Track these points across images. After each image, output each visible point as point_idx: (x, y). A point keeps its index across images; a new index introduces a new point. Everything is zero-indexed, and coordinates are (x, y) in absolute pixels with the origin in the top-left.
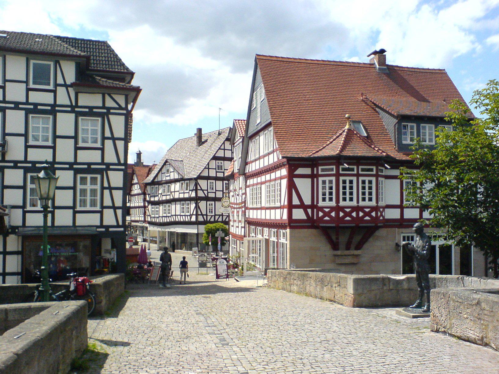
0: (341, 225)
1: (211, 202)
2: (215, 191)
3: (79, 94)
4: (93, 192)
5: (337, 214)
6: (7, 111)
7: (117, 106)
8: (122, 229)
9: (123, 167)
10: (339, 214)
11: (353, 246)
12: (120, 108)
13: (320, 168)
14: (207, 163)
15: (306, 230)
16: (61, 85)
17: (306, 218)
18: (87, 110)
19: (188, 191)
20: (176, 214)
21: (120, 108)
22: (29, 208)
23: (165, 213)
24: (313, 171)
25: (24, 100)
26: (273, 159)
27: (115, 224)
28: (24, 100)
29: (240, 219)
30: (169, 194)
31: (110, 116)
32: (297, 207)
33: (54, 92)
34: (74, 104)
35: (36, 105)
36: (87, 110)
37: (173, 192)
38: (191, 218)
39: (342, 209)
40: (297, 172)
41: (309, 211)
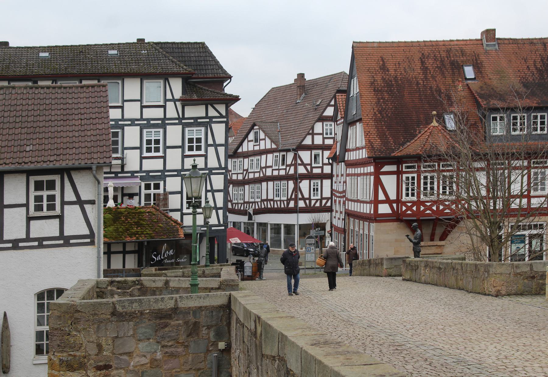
0: (421, 218)
1: (316, 181)
2: (321, 165)
3: (186, 107)
5: (418, 208)
6: (125, 127)
7: (219, 115)
8: (223, 228)
9: (224, 171)
10: (420, 208)
11: (437, 237)
12: (221, 116)
13: (404, 165)
14: (310, 127)
15: (391, 223)
16: (170, 100)
17: (391, 212)
18: (192, 121)
19: (284, 167)
20: (269, 198)
21: (221, 116)
23: (252, 198)
24: (398, 168)
25: (139, 117)
26: (363, 154)
27: (217, 223)
28: (139, 117)
29: (341, 210)
30: (259, 170)
31: (213, 125)
32: (382, 202)
33: (164, 107)
34: (181, 117)
35: (148, 120)
36: (192, 121)
37: (264, 168)
38: (288, 204)
39: (423, 203)
40: (384, 170)
41: (395, 205)
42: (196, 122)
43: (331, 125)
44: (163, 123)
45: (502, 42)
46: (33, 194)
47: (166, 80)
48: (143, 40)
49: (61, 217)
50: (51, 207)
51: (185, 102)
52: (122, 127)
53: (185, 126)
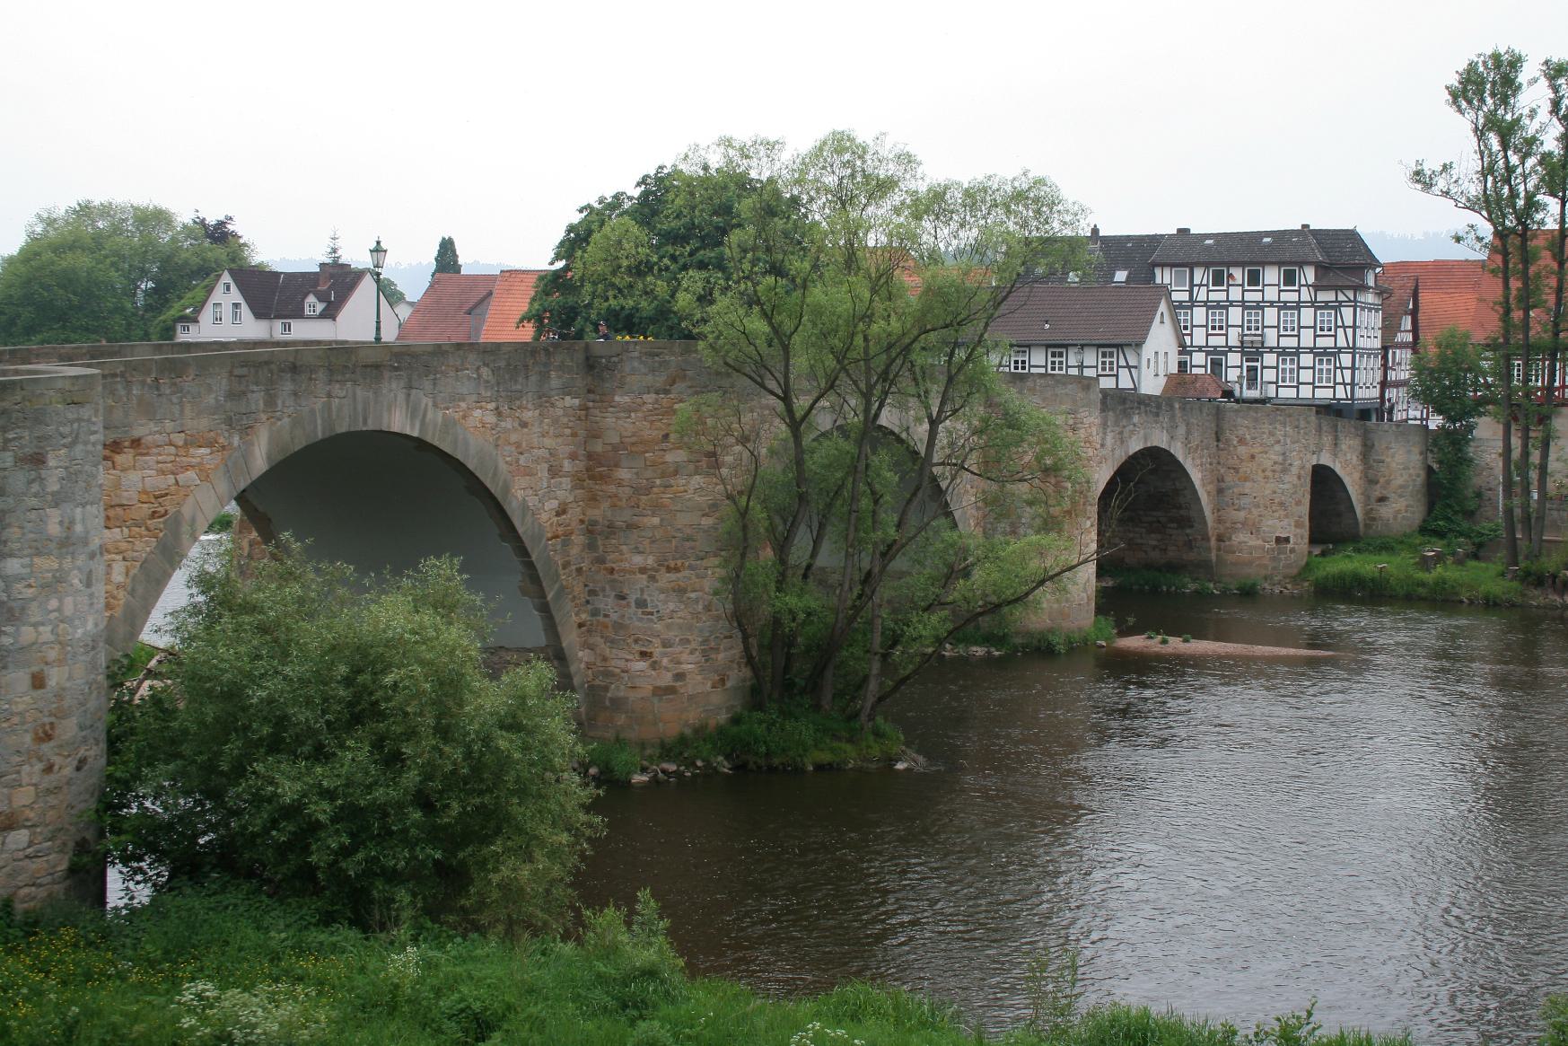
4: (1291, 371)
12: (1350, 301)
21: (1350, 301)
22: (1280, 384)
42: (1326, 305)
43: (1329, 315)
44: (1298, 306)
45: (1106, 240)
46: (1100, 360)
47: (1301, 267)
48: (1186, 231)
49: (1117, 376)
50: (1111, 369)
51: (1317, 287)
52: (1262, 308)
53: (1280, 309)
